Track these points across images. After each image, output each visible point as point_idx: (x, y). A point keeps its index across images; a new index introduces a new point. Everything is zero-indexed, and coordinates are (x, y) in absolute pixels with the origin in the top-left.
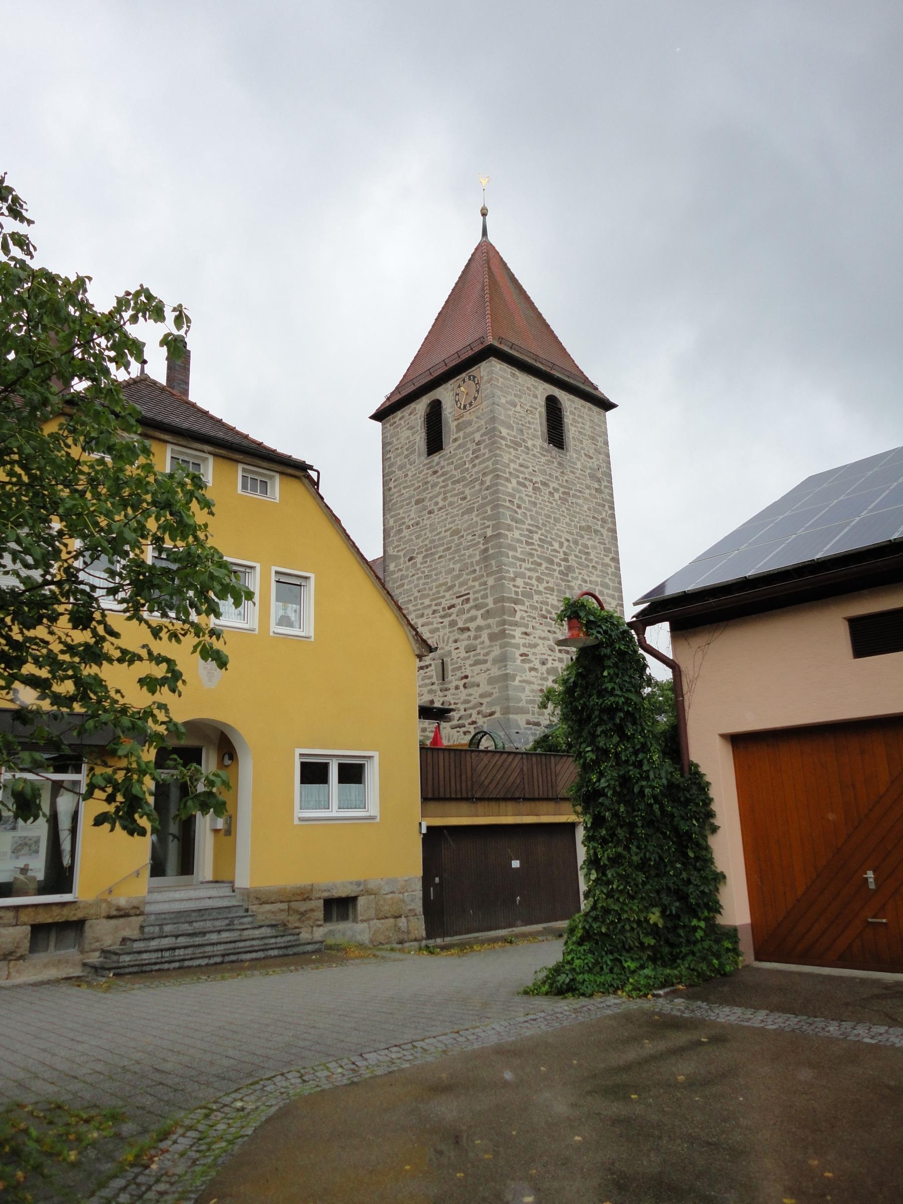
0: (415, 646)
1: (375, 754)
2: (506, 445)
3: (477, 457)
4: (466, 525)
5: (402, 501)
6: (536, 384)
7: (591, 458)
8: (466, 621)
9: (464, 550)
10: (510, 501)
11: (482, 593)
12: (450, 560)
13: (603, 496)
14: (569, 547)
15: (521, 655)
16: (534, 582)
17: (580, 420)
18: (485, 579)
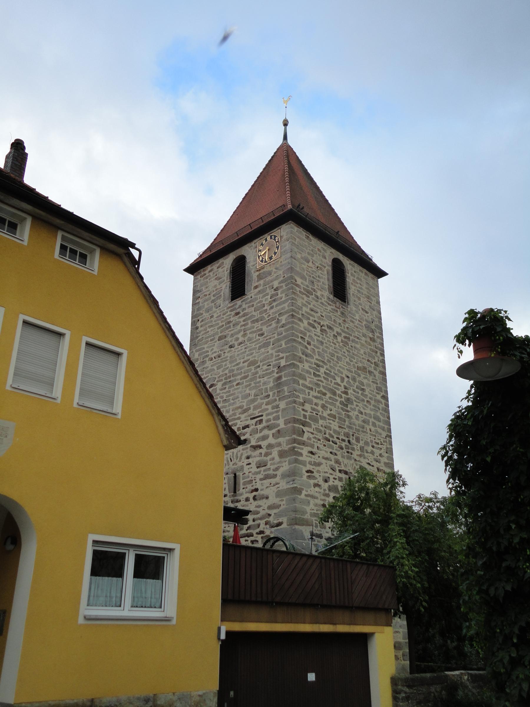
0: (224, 437)
1: (177, 547)
2: (300, 292)
3: (274, 301)
4: (262, 357)
5: (208, 337)
6: (325, 248)
7: (367, 313)
8: (258, 440)
9: (260, 378)
10: (302, 337)
11: (274, 415)
12: (246, 386)
13: (376, 344)
15: (308, 472)
16: (319, 408)
17: (358, 281)
18: (277, 403)
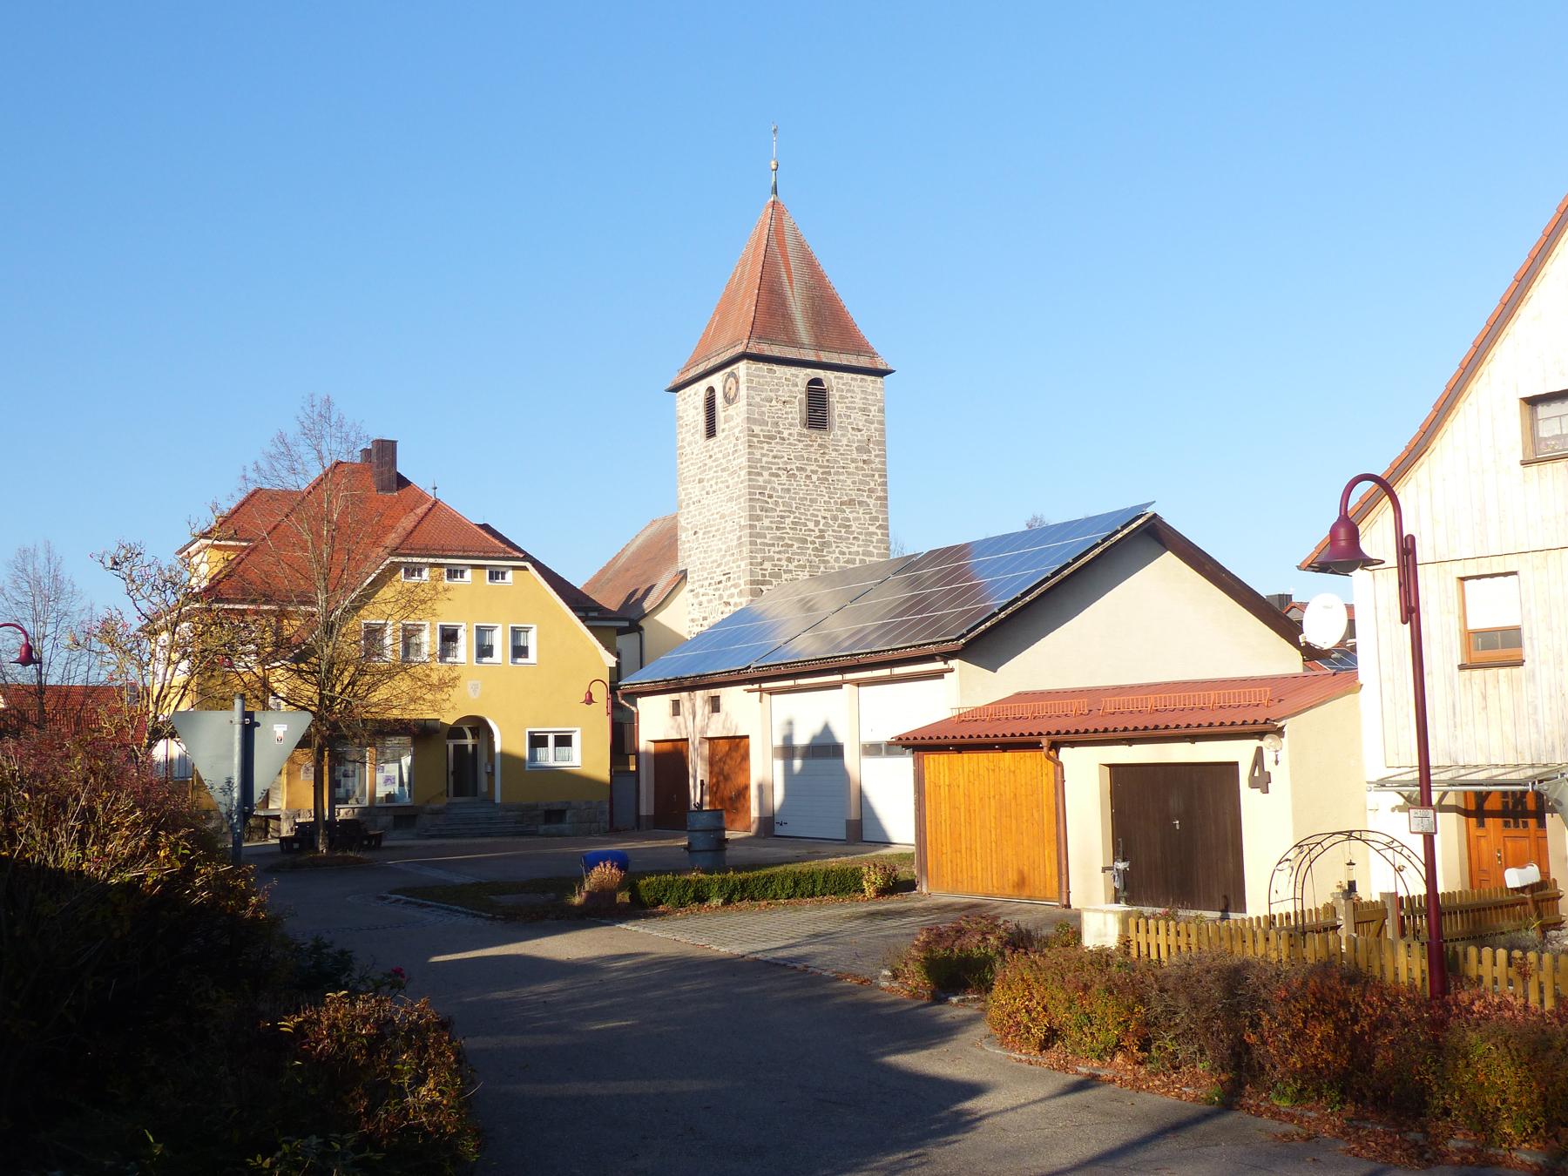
14: (826, 524)
16: (784, 563)
